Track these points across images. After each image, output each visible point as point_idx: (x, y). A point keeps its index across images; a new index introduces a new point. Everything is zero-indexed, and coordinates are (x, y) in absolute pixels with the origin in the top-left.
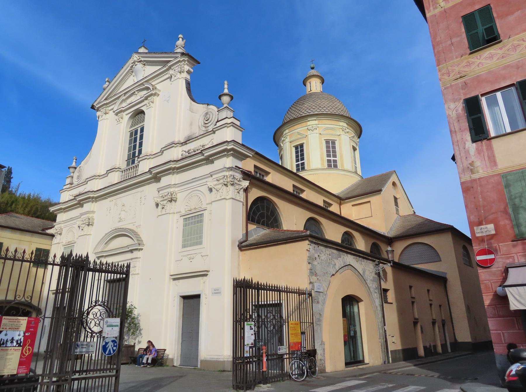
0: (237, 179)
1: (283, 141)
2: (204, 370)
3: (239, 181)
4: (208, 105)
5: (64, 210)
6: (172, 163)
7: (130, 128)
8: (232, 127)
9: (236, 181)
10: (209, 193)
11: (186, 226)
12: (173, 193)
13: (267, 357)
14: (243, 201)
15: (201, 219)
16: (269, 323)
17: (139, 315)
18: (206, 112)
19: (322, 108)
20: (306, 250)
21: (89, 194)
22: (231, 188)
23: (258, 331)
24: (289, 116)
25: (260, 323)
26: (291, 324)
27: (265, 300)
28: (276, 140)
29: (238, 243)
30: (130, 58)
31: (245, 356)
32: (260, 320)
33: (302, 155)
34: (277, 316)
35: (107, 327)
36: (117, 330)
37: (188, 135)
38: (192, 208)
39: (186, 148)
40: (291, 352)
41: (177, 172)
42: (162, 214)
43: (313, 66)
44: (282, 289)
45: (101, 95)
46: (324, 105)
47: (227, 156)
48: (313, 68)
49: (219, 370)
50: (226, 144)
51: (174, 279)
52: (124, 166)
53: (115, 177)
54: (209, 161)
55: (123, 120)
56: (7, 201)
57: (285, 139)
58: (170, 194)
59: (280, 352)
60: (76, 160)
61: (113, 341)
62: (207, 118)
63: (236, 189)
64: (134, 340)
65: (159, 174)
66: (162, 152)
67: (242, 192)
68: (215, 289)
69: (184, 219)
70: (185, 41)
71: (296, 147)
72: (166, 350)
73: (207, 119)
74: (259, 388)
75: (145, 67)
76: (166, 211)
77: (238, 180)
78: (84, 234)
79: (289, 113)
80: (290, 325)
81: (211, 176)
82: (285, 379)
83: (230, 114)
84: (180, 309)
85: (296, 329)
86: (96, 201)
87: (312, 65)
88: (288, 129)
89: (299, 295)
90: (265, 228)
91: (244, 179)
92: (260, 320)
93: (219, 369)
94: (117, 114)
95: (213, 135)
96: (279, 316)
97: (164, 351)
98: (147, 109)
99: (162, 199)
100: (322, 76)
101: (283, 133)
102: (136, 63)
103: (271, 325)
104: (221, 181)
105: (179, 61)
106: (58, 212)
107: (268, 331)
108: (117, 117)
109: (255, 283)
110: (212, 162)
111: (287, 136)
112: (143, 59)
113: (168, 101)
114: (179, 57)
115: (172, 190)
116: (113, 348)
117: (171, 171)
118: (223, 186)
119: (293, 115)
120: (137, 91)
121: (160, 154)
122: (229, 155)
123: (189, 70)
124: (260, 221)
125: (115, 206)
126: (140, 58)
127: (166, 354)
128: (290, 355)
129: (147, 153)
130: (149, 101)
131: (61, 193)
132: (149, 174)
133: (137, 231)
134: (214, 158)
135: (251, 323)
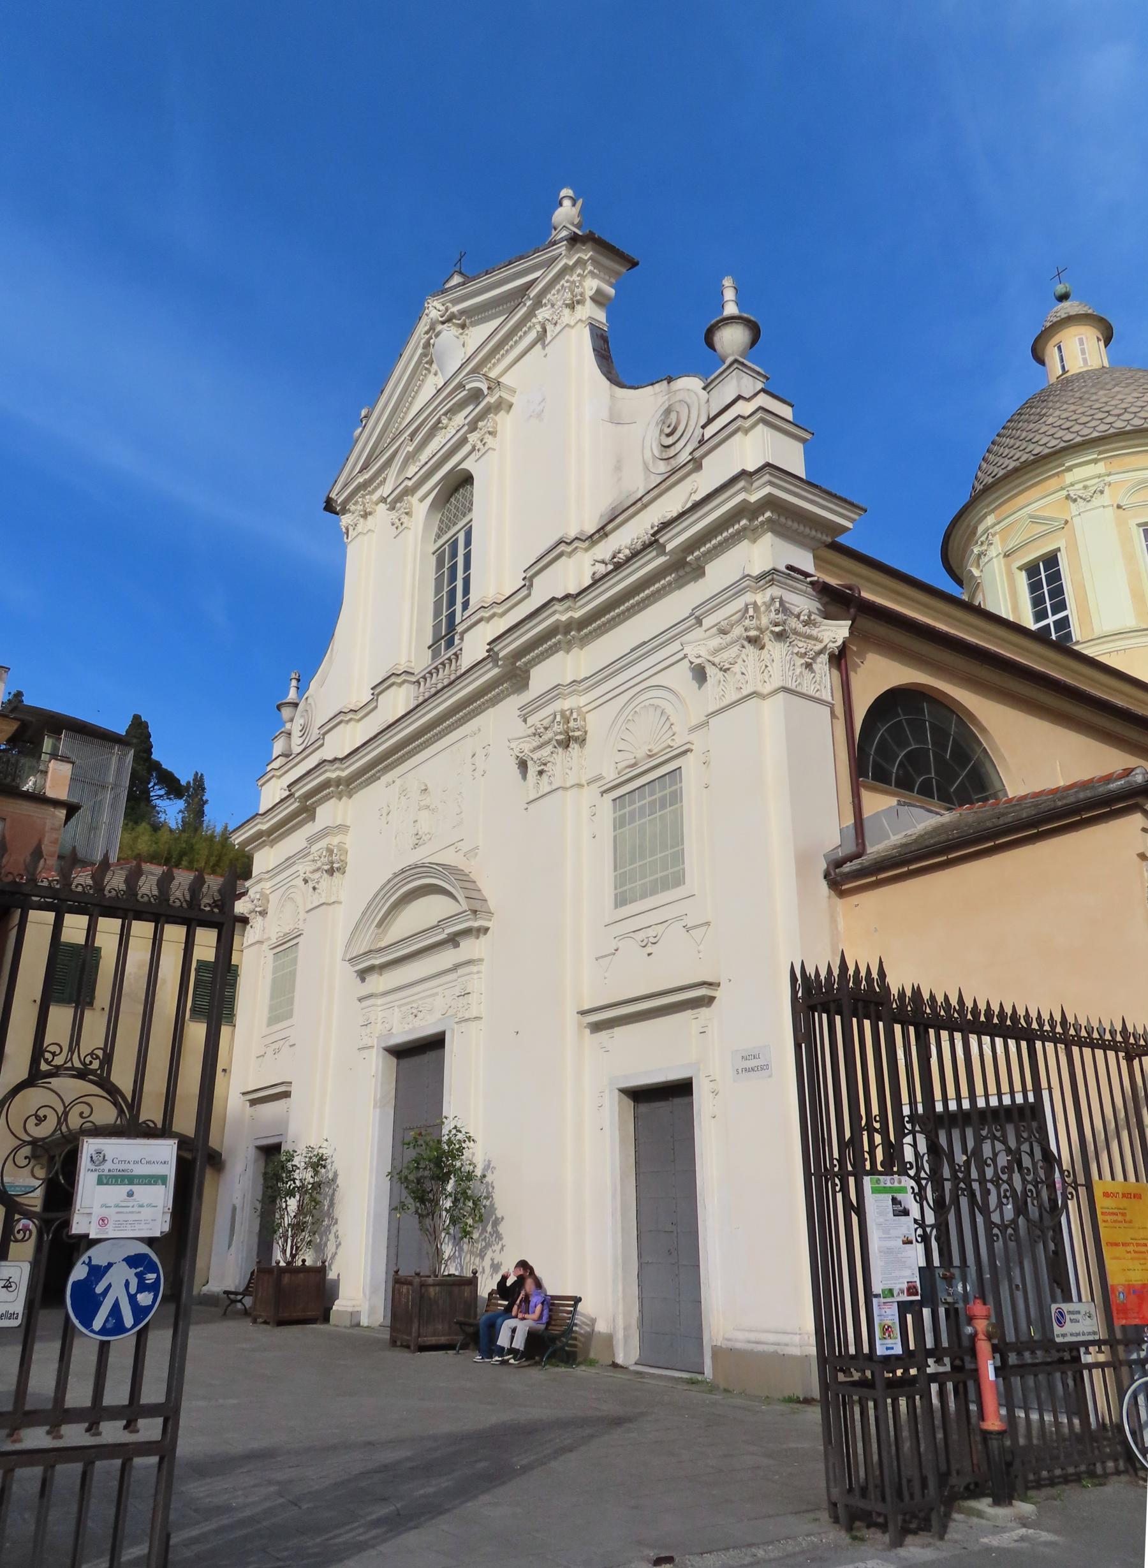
0: (798, 616)
1: (979, 556)
2: (726, 1391)
3: (806, 623)
4: (670, 380)
5: (269, 836)
6: (557, 607)
7: (435, 541)
8: (761, 426)
9: (793, 623)
10: (697, 686)
11: (622, 825)
12: (572, 713)
13: (998, 1356)
14: (829, 699)
15: (674, 788)
16: (990, 1186)
17: (488, 1166)
18: (667, 406)
19: (1116, 415)
20: (1137, 859)
21: (326, 771)
22: (776, 650)
23: (942, 1226)
24: (991, 468)
25: (948, 1186)
26: (1106, 1195)
27: (964, 1092)
28: (951, 562)
29: (826, 866)
30: (420, 318)
31: (880, 1351)
32: (946, 1173)
33: (1058, 592)
34: (1032, 1154)
35: (100, 1182)
36: (160, 1203)
37: (611, 505)
38: (638, 756)
39: (605, 550)
40: (1119, 1335)
41: (582, 639)
42: (539, 795)
43: (1063, 291)
44: (1041, 1025)
45: (347, 459)
46: (1124, 405)
47: (752, 534)
48: (1063, 297)
49: (786, 1396)
50: (742, 484)
51: (597, 1027)
52: (421, 661)
53: (398, 701)
54: (688, 569)
55: (412, 519)
56: (169, 853)
57: (984, 547)
58: (558, 718)
59: (1065, 1333)
60: (298, 680)
61: (133, 1261)
62: (669, 427)
63: (797, 654)
64: (478, 1258)
65: (520, 659)
66: (528, 583)
67: (822, 664)
68: (744, 1054)
69: (614, 800)
70: (580, 203)
71: (1031, 570)
72: (580, 1300)
73: (668, 431)
74: (975, 1520)
75: (467, 334)
76: (551, 783)
77: (802, 618)
78: (321, 902)
79: (991, 457)
80: (1101, 1203)
81: (699, 622)
82: (1104, 1468)
83: (748, 384)
84: (623, 1142)
85: (1131, 1222)
86: (349, 792)
87: (1061, 286)
88: (993, 511)
89: (1129, 1059)
90: (935, 806)
91: (827, 616)
92: (946, 1173)
93: (787, 1393)
94: (392, 508)
95: (694, 476)
96: (1038, 1154)
97: (575, 1306)
98: (476, 461)
99: (536, 742)
100: (1102, 316)
101: (974, 532)
102: (439, 327)
103: (1006, 1197)
104: (738, 631)
105: (566, 270)
106: (254, 847)
107: (989, 1224)
108: (394, 515)
109: (902, 994)
110: (699, 572)
111: (990, 537)
112: (455, 309)
113: (539, 415)
114: (564, 253)
115: (566, 704)
116: (132, 1299)
117: (559, 637)
118: (743, 647)
119: (1007, 462)
120: (445, 414)
121: (524, 592)
122: (757, 528)
123: (599, 291)
124: (914, 782)
125: (402, 797)
126: (447, 310)
127: (583, 1315)
128: (1121, 1348)
129: (483, 601)
130: (483, 432)
131: (262, 785)
132: (491, 665)
133: (467, 871)
134: (704, 554)
135: (896, 1184)
